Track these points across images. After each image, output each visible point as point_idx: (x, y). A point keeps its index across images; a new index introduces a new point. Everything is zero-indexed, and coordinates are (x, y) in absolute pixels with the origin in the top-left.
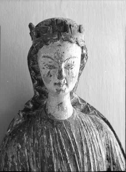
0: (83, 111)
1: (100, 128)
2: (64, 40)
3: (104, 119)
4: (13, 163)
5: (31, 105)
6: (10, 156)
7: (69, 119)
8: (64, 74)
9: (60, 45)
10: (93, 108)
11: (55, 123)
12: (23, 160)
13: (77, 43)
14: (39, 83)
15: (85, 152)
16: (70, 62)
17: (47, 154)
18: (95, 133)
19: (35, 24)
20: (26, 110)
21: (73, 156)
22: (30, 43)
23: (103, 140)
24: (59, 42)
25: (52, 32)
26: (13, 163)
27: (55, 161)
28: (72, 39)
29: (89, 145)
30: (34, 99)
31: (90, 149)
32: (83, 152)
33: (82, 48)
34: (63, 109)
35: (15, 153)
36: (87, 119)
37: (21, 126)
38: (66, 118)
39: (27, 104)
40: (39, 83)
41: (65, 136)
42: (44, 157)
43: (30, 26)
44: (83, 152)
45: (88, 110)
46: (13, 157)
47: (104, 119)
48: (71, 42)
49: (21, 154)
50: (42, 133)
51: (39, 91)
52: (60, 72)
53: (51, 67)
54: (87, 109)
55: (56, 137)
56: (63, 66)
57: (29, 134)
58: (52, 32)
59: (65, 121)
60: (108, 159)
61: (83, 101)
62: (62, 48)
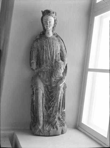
0: (56, 37)
1: (59, 41)
2: (48, 15)
3: (61, 39)
4: (35, 47)
5: (42, 33)
6: (34, 45)
7: (50, 37)
8: (48, 24)
9: (47, 16)
10: (59, 36)
11: (47, 38)
12: (37, 46)
13: (52, 16)
14: (44, 28)
15: (53, 46)
16: (50, 21)
17: (43, 45)
18: (57, 42)
19: (43, 11)
20: (41, 34)
21: (49, 46)
22: (42, 15)
23: (60, 44)
24: (47, 16)
25: (47, 13)
26: (35, 47)
27: (45, 46)
28: (51, 15)
29: (54, 44)
30: (43, 31)
31: (55, 45)
32: (52, 45)
33: (54, 18)
34: (49, 34)
35: (36, 44)
36: (56, 38)
37: (38, 38)
38: (50, 37)
39: (41, 33)
40: (44, 28)
41: (48, 41)
42: (42, 45)
43: (42, 11)
44: (52, 45)
45: (57, 37)
46: (35, 45)
47: (61, 39)
48: (50, 16)
49: (37, 45)
50: (43, 40)
51: (44, 29)
52: (47, 23)
53: (46, 22)
54: (57, 36)
55: (46, 42)
56: (48, 22)
57: (40, 40)
58: (47, 13)
59: (49, 37)
60: (61, 50)
61: (56, 34)
62: (48, 17)
